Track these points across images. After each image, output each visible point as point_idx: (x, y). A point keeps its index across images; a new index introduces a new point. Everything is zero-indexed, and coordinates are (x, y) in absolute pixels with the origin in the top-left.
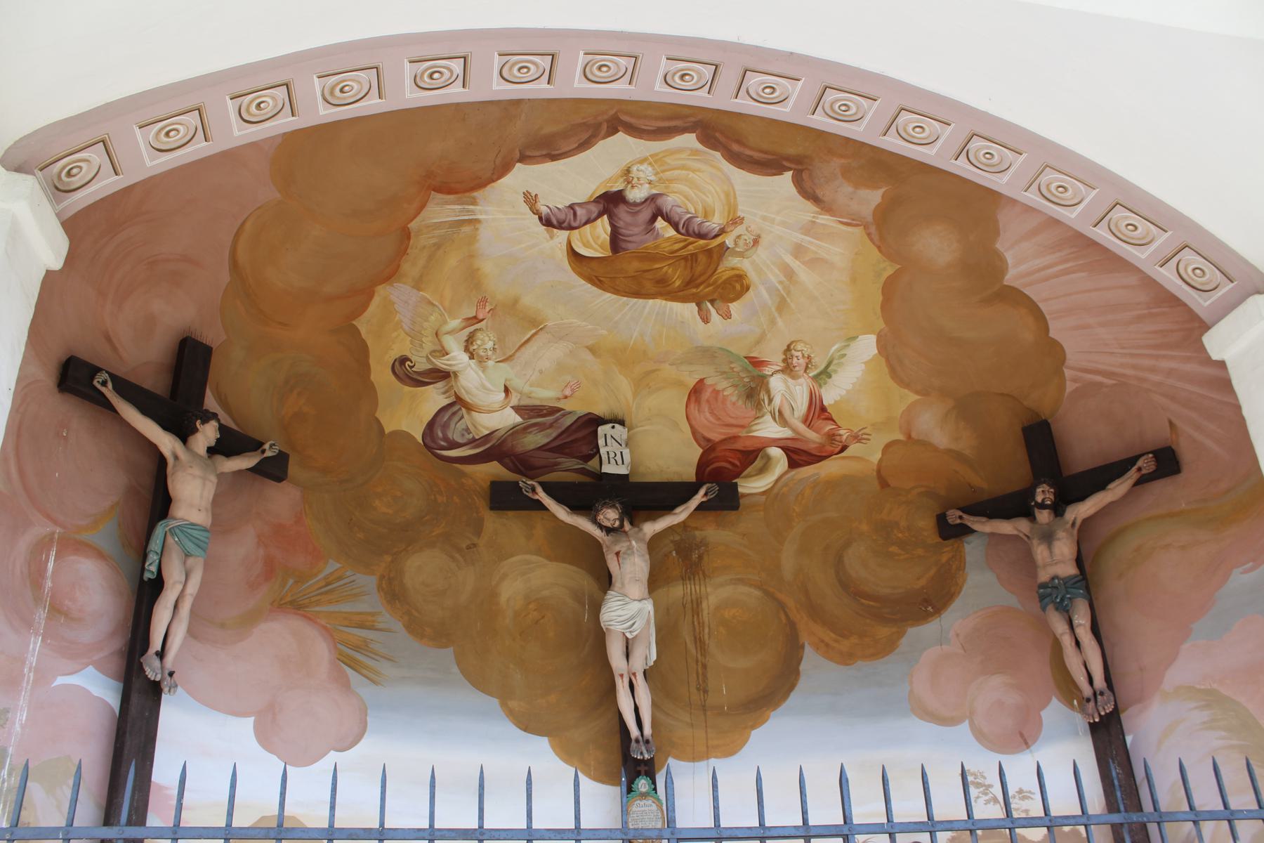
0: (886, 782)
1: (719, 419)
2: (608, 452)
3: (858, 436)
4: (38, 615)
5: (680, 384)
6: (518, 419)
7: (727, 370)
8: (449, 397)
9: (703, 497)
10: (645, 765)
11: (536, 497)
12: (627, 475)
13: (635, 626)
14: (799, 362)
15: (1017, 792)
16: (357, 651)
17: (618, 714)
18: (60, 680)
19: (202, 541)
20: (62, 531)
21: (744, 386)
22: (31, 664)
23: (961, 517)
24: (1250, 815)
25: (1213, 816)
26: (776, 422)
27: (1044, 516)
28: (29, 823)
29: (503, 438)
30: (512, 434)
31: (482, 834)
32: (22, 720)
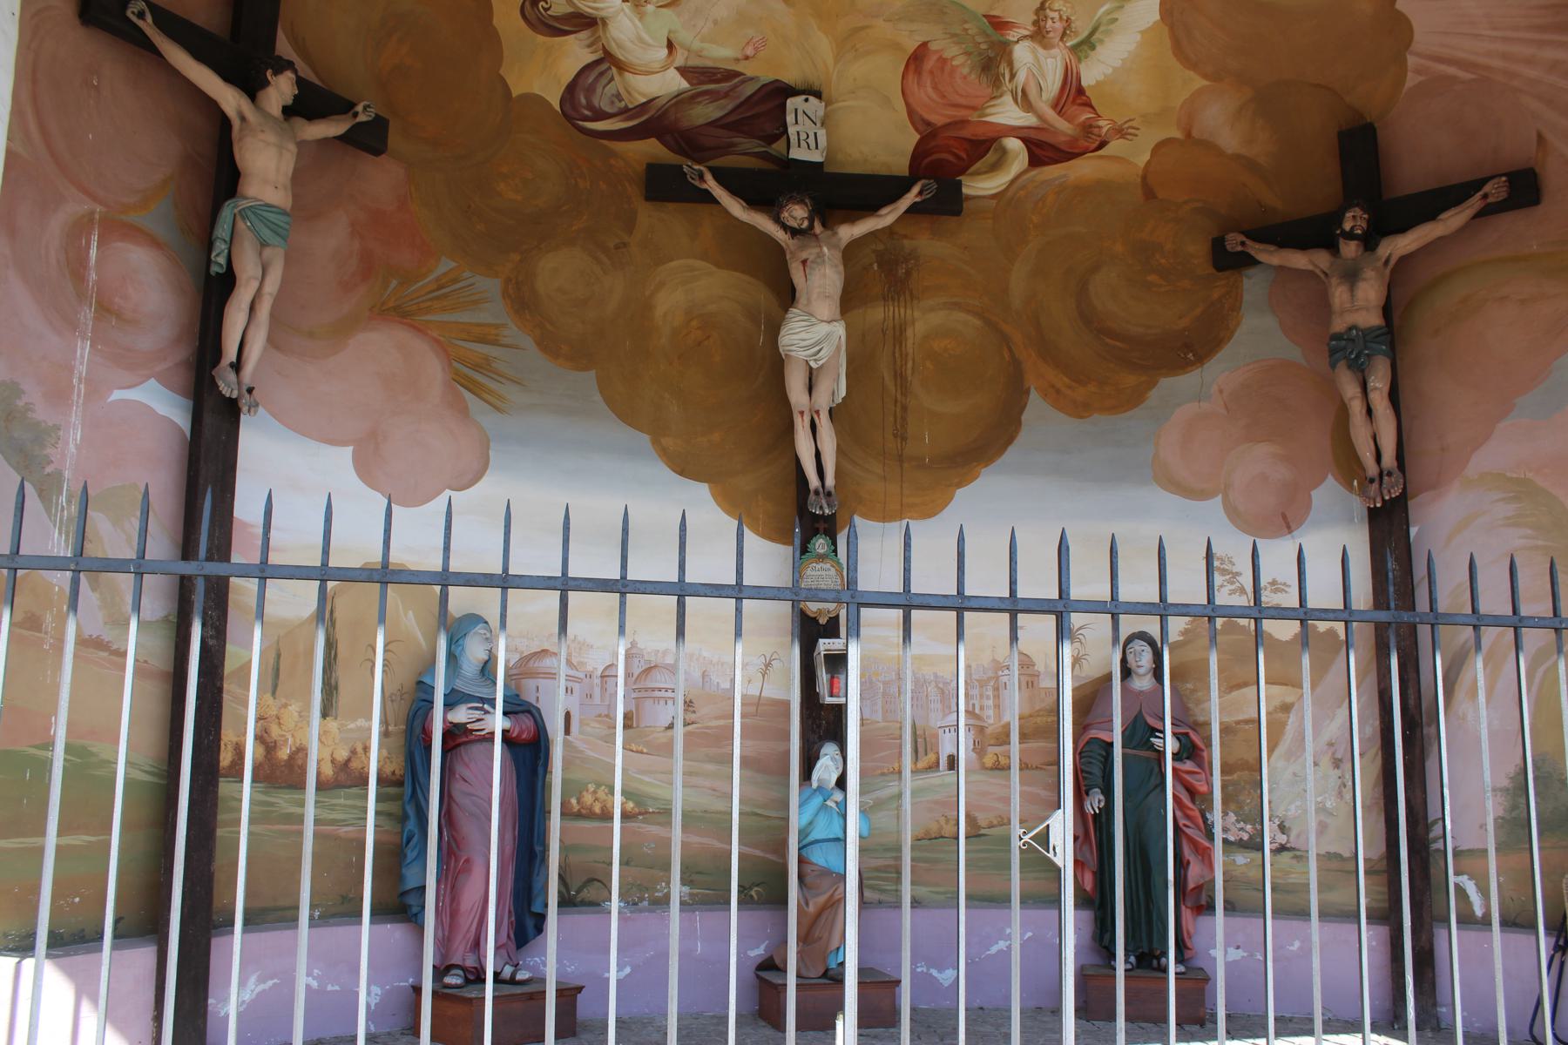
0: (1114, 554)
1: (943, 97)
2: (798, 133)
3: (1123, 130)
4: (83, 314)
5: (896, 46)
6: (685, 85)
7: (958, 32)
8: (596, 52)
9: (916, 196)
10: (825, 522)
11: (704, 186)
12: (822, 163)
13: (820, 354)
14: (1054, 26)
15: (1269, 583)
16: (477, 371)
17: (794, 461)
18: (117, 395)
19: (281, 227)
20: (104, 209)
21: (980, 54)
22: (81, 374)
23: (1243, 244)
24: (1542, 623)
25: (1497, 621)
26: (1019, 106)
27: (1350, 249)
28: (91, 636)
29: (663, 109)
30: (676, 103)
31: (625, 586)
32: (76, 440)
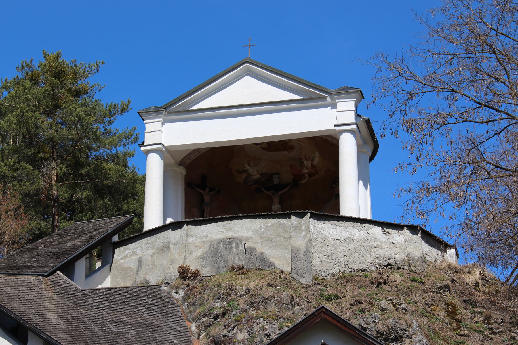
6: (260, 176)
